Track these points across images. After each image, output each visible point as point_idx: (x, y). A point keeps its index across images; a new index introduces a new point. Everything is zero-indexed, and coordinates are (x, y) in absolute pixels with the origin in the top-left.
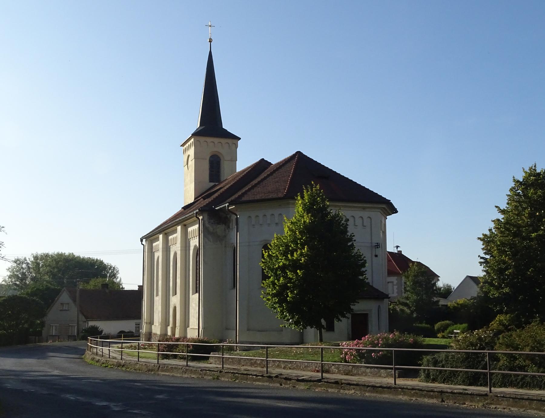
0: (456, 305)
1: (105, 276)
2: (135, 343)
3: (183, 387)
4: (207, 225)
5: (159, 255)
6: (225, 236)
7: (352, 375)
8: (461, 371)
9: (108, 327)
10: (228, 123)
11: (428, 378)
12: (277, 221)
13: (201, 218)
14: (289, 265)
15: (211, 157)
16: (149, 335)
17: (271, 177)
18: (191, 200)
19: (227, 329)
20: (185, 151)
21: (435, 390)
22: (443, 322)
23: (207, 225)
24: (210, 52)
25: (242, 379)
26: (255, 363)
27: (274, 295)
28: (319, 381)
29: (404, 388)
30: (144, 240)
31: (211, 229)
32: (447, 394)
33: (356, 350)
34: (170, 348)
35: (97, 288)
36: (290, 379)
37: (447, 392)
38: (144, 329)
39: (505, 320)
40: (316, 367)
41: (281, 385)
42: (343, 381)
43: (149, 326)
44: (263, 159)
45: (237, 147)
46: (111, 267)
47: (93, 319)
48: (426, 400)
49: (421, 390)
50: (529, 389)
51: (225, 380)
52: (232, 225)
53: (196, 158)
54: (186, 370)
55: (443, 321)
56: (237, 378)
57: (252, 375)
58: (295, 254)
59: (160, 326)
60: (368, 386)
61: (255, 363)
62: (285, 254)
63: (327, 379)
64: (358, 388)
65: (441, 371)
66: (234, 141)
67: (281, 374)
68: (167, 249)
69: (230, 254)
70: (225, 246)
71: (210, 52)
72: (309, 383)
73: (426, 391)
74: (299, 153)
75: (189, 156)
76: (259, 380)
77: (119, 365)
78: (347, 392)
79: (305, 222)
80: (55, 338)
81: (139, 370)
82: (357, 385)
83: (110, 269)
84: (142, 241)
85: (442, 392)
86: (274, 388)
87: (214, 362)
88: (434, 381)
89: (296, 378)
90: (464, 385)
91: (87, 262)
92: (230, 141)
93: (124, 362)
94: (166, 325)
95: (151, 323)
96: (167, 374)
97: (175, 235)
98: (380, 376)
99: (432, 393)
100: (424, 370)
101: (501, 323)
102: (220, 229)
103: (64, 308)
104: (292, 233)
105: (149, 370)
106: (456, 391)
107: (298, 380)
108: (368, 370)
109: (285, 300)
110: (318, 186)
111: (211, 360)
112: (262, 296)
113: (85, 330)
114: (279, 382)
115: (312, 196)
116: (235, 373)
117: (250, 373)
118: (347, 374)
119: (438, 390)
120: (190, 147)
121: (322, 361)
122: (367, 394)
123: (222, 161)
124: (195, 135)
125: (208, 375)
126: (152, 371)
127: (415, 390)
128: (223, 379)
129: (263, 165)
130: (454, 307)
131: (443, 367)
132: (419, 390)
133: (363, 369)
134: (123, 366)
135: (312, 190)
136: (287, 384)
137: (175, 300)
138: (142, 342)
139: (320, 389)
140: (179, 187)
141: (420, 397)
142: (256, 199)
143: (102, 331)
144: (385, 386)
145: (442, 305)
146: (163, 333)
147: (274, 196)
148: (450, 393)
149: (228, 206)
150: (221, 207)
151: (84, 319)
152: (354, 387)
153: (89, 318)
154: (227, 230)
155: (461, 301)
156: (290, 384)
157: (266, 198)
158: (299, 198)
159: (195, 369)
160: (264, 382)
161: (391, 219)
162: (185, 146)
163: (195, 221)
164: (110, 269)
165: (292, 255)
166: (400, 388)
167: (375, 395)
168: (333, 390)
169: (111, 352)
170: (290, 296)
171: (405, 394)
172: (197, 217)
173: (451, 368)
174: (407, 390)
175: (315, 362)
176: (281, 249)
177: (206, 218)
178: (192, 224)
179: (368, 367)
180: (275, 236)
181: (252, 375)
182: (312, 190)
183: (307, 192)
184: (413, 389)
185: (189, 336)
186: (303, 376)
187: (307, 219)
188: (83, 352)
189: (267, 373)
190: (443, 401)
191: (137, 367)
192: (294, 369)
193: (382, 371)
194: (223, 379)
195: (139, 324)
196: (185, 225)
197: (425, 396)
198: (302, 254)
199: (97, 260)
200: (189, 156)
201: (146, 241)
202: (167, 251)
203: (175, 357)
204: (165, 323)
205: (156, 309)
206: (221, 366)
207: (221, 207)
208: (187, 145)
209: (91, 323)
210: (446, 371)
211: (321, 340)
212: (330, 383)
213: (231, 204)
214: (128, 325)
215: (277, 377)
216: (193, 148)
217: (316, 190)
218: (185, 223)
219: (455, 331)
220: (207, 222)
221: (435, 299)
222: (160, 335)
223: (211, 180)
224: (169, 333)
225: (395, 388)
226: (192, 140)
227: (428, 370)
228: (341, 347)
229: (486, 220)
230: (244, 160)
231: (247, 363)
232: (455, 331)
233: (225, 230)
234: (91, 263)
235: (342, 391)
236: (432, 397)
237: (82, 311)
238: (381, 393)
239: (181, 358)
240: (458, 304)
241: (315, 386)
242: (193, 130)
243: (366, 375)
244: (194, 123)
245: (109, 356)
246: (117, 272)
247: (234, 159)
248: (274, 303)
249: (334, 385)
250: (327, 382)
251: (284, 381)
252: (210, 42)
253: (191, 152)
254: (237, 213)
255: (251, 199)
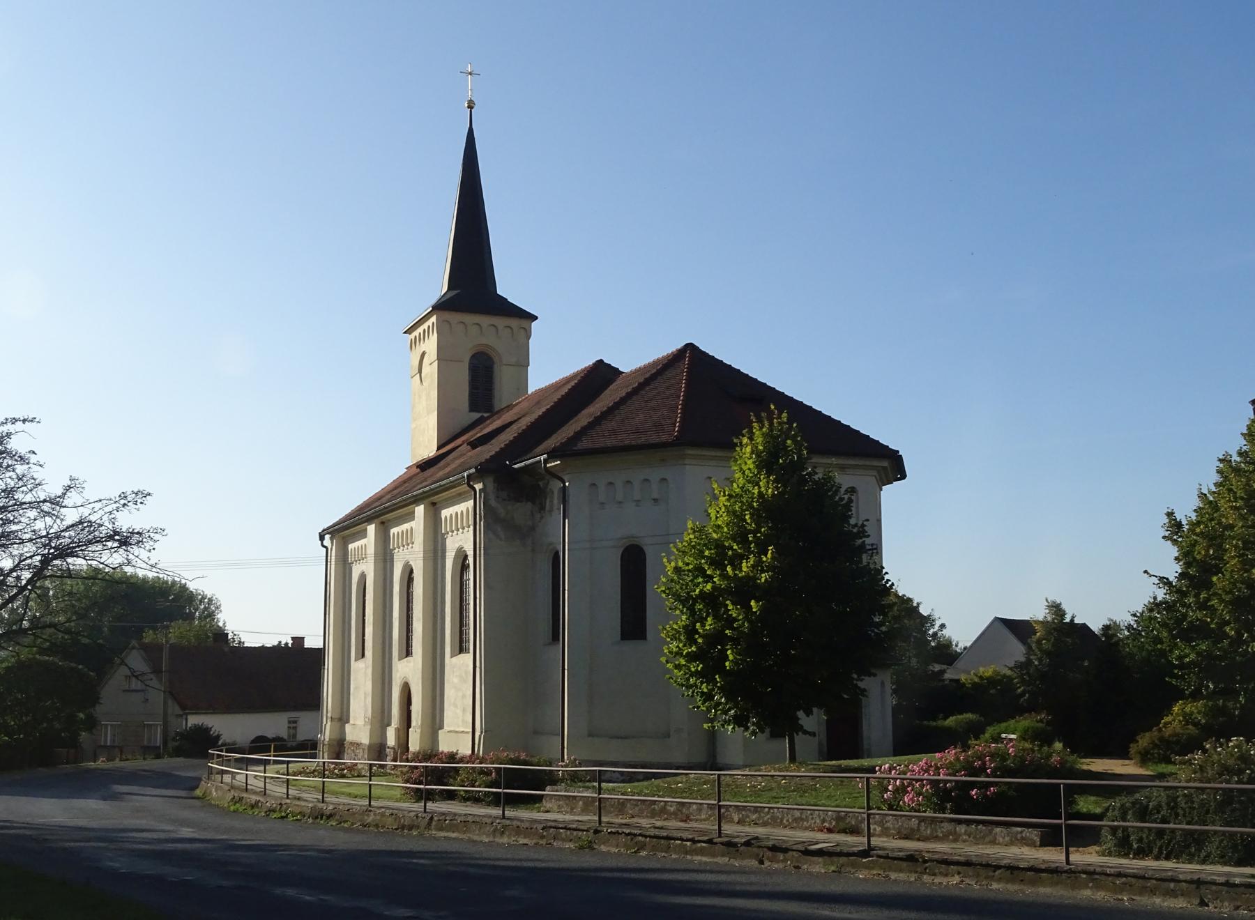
0: (976, 680)
1: (191, 617)
2: (311, 764)
3: (536, 868)
4: (493, 503)
5: (365, 567)
6: (533, 528)
7: (919, 840)
8: (1216, 832)
9: (232, 727)
10: (508, 286)
11: (1124, 846)
12: (655, 496)
13: (478, 486)
14: (728, 588)
15: (473, 357)
16: (339, 747)
17: (635, 398)
18: (429, 449)
19: (536, 732)
20: (413, 344)
21: (1181, 877)
22: (960, 717)
23: (493, 503)
24: (471, 131)
25: (654, 848)
26: (663, 810)
27: (691, 658)
28: (865, 853)
29: (1094, 873)
30: (327, 537)
31: (502, 512)
32: (1214, 888)
33: (931, 782)
34: (439, 776)
35: (185, 642)
36: (785, 850)
37: (1214, 883)
38: (327, 734)
39: (1199, 713)
40: (824, 821)
41: (761, 862)
42: (927, 856)
43: (337, 725)
44: (601, 361)
45: (529, 336)
46: (204, 597)
47: (197, 710)
48: (1158, 900)
49: (1143, 877)
50: (1142, 859)
51: (611, 853)
52: (552, 502)
53: (441, 358)
54: (504, 827)
55: (961, 713)
56: (642, 847)
57: (681, 839)
58: (744, 565)
59: (369, 727)
60: (998, 867)
61: (663, 810)
62: (717, 563)
63: (880, 849)
64: (970, 871)
65: (1160, 833)
66: (524, 323)
67: (757, 838)
68: (385, 557)
69: (547, 567)
70: (533, 550)
71: (471, 131)
72: (835, 859)
73: (1156, 879)
74: (690, 347)
75: (423, 354)
76: (701, 852)
77: (319, 815)
78: (944, 880)
79: (761, 494)
80: (111, 751)
81: (377, 826)
82: (968, 864)
83: (201, 601)
84: (322, 538)
85: (1199, 883)
86: (742, 871)
87: (555, 808)
88: (1141, 853)
89: (801, 847)
90: (1225, 864)
91: (153, 587)
92: (514, 323)
93: (331, 807)
94: (382, 720)
95: (343, 718)
96: (454, 835)
97: (412, 524)
98: (994, 842)
99: (1172, 885)
100: (1114, 830)
101: (1188, 719)
102: (521, 512)
103: (133, 687)
104: (677, 525)
105: (403, 827)
106: (1237, 881)
107: (807, 853)
108: (962, 829)
109: (721, 669)
110: (785, 415)
111: (547, 804)
112: (663, 659)
113: (177, 734)
114: (756, 857)
115: (772, 436)
116: (635, 835)
117: (675, 834)
118: (906, 838)
119: (1188, 877)
120: (426, 334)
121: (869, 808)
122: (995, 886)
123: (496, 368)
124: (439, 307)
125: (563, 840)
126: (411, 828)
127: (1126, 876)
128: (603, 848)
129: (600, 375)
130: (974, 684)
131: (1164, 821)
132: (1135, 876)
133: (947, 827)
134: (330, 816)
135: (771, 424)
136: (778, 862)
137: (409, 670)
138: (324, 758)
139: (866, 872)
140: (409, 424)
141: (1141, 894)
142: (609, 445)
143: (218, 737)
144: (1043, 867)
145: (951, 680)
146: (377, 740)
147: (654, 439)
148: (1222, 884)
149: (546, 461)
150: (527, 462)
151: (178, 711)
152: (960, 868)
153: (188, 707)
154: (538, 516)
155: (987, 671)
156: (785, 860)
157: (634, 443)
158: (745, 440)
159: (527, 825)
160: (714, 856)
161: (890, 494)
162: (416, 333)
163: (465, 492)
164: (201, 601)
165: (737, 567)
166: (1085, 872)
167: (1016, 887)
168: (902, 876)
169: (262, 779)
170: (731, 657)
171: (1098, 887)
172: (469, 485)
173: (1188, 823)
174: (1103, 878)
175: (783, 805)
176: (707, 553)
177: (491, 486)
178: (459, 498)
179: (960, 822)
180: (690, 524)
181: (681, 839)
182: (771, 424)
183: (761, 428)
184: (1119, 875)
185: (445, 746)
186: (817, 843)
187: (767, 487)
188: (193, 784)
189: (720, 836)
190: (1203, 903)
191: (370, 819)
192: (765, 824)
193: (998, 830)
194: (603, 848)
195: (295, 722)
196: (434, 504)
197: (1153, 892)
198: (758, 565)
199: (174, 582)
200: (423, 354)
201: (331, 539)
202: (385, 561)
203: (451, 796)
204: (381, 718)
205: (356, 688)
206: (596, 818)
207: (527, 462)
208: (420, 330)
209: (194, 720)
210: (1173, 831)
211: (793, 759)
212: (895, 859)
213: (552, 455)
214: (273, 724)
215: (748, 844)
216: (434, 338)
217: (780, 424)
218: (434, 499)
219: (1004, 736)
220: (492, 497)
221: (937, 667)
222: (370, 746)
223: (473, 407)
224: (391, 740)
225: (1070, 872)
226: (434, 319)
227: (1125, 829)
228: (878, 774)
229: (1188, 485)
230: (549, 364)
231: (641, 811)
232: (1004, 736)
233: (532, 514)
234: (161, 588)
235: (926, 878)
236: (1173, 894)
237: (172, 694)
238: (1033, 883)
239: (465, 799)
240: (981, 677)
241: (853, 865)
242: (434, 299)
243: (955, 841)
244: (436, 281)
245: (252, 792)
246: (217, 608)
247: (523, 363)
248: (692, 675)
249: (904, 864)
250: (887, 857)
251: (769, 854)
252: (470, 107)
253: (431, 345)
254: (565, 478)
255: (597, 446)
